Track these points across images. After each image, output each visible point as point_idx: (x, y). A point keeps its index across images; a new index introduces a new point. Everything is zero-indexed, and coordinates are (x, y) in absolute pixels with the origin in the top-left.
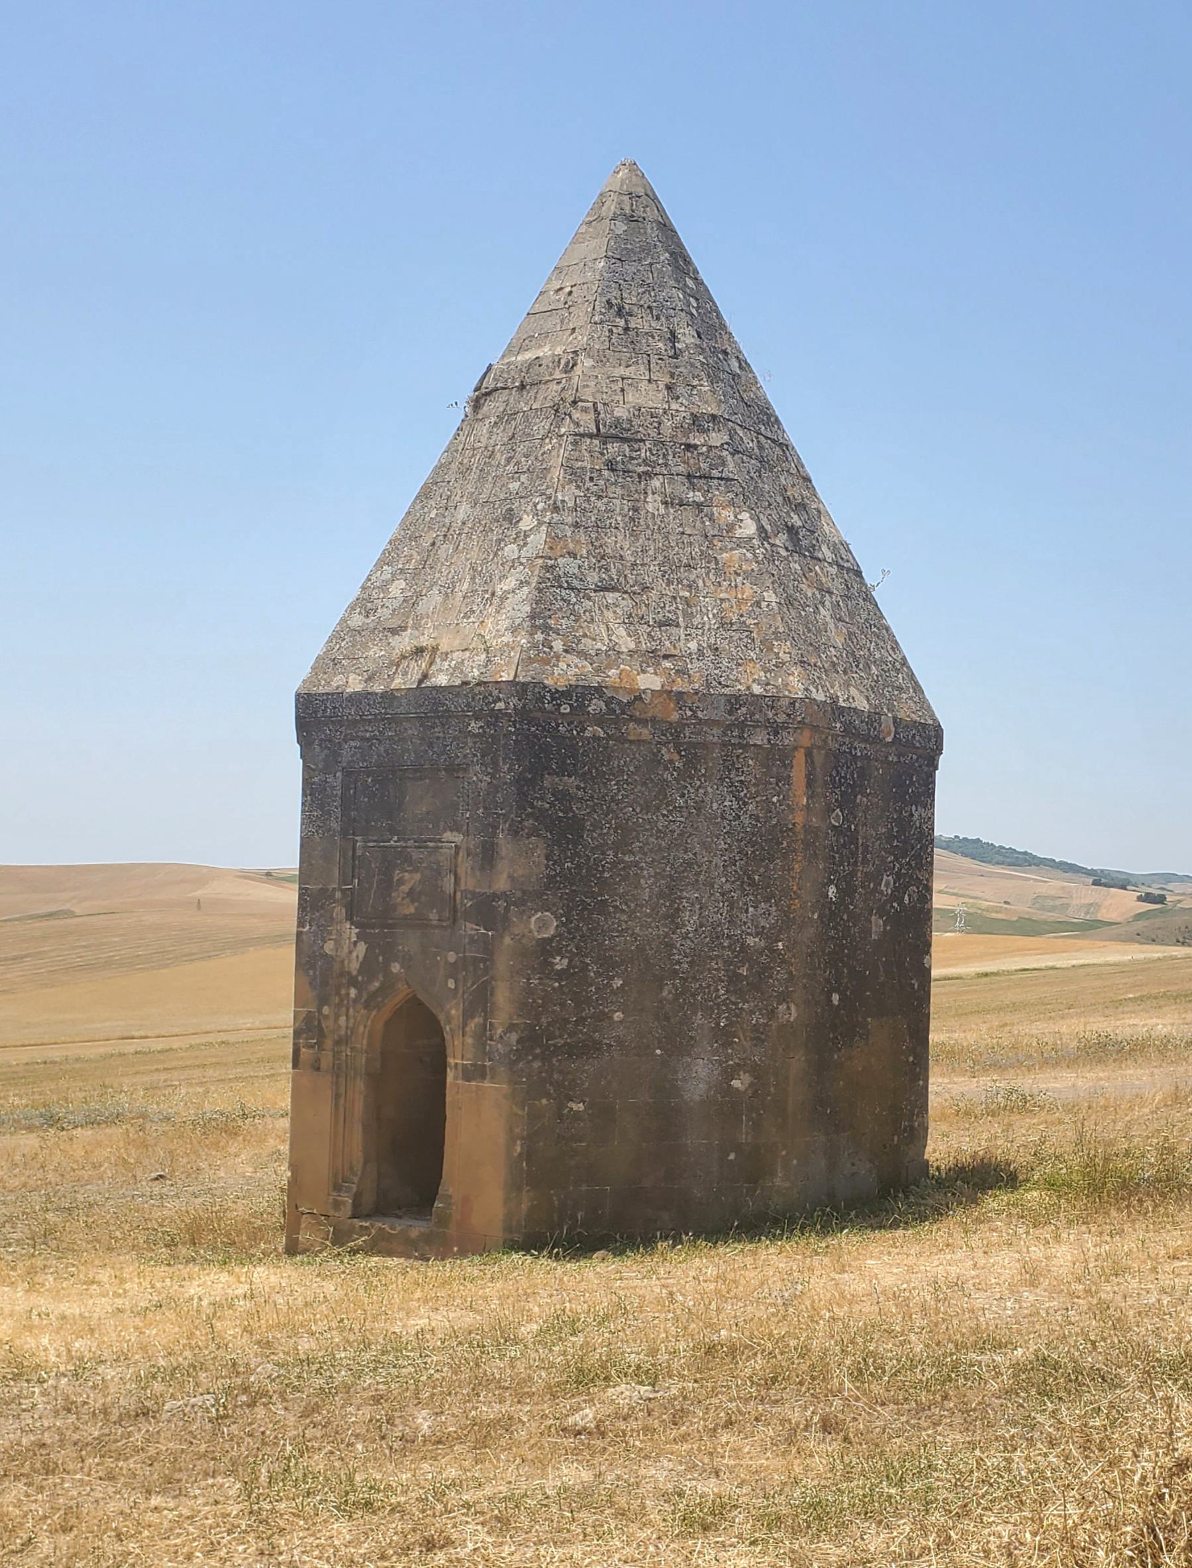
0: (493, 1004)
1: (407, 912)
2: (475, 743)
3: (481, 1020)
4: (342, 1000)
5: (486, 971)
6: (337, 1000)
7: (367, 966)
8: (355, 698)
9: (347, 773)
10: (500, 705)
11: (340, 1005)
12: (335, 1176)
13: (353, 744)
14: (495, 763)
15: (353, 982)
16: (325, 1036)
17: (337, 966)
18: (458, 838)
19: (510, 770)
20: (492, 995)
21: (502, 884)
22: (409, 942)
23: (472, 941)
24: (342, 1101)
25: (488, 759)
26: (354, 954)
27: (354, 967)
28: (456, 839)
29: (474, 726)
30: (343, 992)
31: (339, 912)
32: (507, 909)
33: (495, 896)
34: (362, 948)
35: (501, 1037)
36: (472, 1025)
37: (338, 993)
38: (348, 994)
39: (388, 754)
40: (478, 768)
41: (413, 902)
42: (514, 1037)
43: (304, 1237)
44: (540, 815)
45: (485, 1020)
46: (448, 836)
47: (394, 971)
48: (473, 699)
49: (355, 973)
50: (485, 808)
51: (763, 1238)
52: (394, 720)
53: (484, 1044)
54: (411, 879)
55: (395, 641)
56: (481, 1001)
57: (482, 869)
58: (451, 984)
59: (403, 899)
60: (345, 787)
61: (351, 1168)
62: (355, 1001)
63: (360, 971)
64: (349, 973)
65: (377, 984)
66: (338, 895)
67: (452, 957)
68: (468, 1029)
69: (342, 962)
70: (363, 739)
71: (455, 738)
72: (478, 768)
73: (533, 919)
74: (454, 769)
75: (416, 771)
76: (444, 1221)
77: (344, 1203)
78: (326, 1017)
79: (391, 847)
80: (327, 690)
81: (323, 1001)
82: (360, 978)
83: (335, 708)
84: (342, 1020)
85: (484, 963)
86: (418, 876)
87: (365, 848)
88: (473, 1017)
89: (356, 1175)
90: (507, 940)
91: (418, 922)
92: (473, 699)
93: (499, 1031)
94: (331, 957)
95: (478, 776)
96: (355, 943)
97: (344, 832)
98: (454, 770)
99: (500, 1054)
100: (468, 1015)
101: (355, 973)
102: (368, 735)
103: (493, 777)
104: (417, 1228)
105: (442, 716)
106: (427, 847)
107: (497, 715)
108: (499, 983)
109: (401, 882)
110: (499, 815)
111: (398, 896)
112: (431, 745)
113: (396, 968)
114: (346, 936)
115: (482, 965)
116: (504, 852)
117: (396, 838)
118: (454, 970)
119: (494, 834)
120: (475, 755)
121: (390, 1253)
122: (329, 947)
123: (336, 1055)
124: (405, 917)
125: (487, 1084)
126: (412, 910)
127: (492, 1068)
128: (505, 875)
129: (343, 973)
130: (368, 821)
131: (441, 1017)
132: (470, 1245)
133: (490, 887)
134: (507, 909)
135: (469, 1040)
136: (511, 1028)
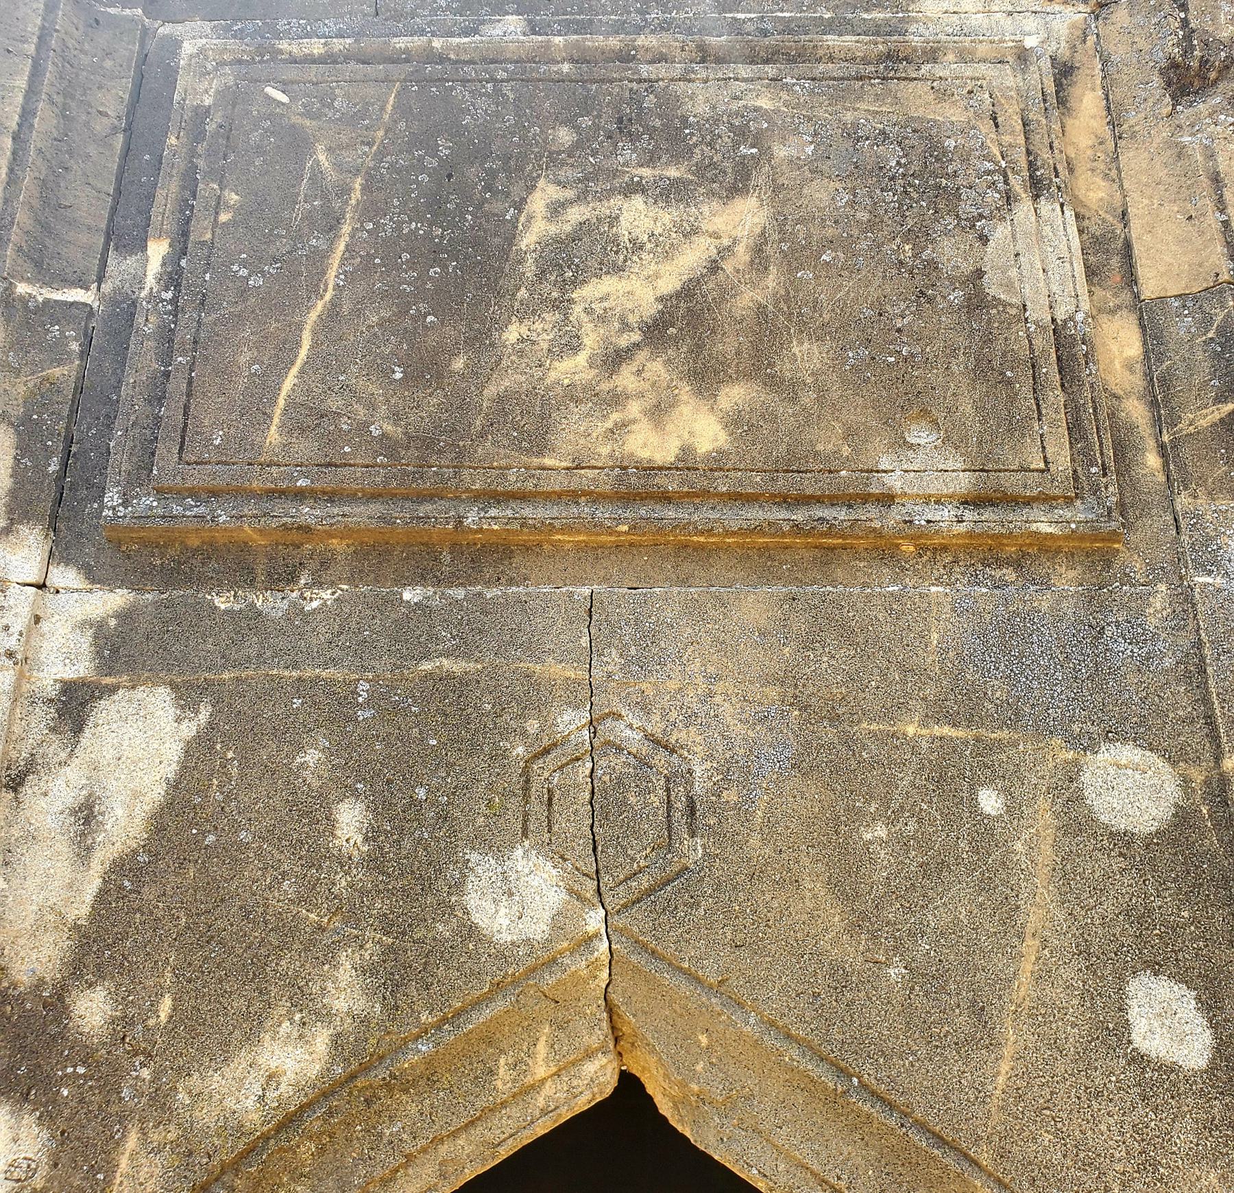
1: (650, 445)
22: (697, 678)
41: (705, 378)
54: (668, 244)
59: (614, 359)
63: (98, 947)
65: (293, 1056)
82: (92, 1010)
86: (742, 219)
91: (798, 524)
96: (74, 706)
109: (573, 259)
113: (520, 897)
124: (638, 487)
126: (702, 429)
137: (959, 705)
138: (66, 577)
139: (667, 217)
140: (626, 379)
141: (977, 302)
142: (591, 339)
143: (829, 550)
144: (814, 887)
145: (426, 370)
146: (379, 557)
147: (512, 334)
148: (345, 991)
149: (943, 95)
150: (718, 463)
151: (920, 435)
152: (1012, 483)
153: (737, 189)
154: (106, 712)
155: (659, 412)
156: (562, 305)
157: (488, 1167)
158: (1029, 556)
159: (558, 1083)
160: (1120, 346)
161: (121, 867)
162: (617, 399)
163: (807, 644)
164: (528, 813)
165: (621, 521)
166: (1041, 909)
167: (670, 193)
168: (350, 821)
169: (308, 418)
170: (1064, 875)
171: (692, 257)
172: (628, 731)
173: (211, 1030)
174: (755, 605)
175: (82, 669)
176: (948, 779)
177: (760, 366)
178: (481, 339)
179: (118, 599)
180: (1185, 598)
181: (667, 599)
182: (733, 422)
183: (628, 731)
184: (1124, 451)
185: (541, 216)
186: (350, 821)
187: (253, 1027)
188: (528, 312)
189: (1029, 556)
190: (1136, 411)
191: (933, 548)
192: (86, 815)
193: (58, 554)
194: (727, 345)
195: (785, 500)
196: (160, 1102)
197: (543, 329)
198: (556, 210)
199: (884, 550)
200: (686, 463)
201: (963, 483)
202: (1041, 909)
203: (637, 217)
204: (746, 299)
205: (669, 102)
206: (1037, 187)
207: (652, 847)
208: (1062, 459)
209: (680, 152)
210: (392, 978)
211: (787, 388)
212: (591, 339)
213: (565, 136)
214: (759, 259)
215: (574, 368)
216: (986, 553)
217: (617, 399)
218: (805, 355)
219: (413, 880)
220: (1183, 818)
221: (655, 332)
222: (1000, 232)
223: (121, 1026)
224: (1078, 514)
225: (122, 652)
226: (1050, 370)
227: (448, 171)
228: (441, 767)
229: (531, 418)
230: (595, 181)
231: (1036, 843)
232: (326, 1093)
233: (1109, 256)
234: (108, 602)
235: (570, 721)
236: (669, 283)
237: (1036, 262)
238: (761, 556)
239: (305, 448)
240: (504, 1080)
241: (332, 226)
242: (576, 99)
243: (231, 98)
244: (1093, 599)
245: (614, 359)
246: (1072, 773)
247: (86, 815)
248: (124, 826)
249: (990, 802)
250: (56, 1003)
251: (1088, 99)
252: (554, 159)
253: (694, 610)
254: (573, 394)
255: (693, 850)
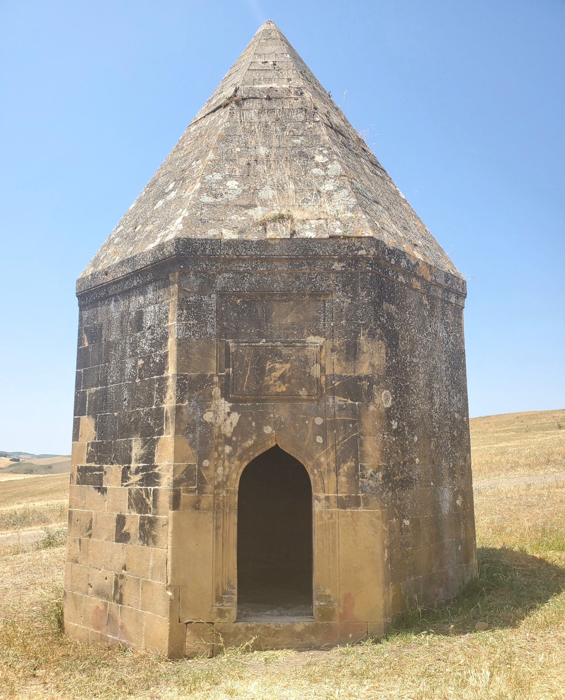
0: (362, 452)
1: (279, 390)
2: (337, 277)
3: (353, 464)
4: (219, 455)
5: (355, 429)
6: (216, 455)
7: (239, 430)
8: (230, 244)
9: (222, 294)
10: (362, 252)
11: (219, 458)
12: (217, 589)
13: (226, 275)
14: (355, 292)
15: (228, 441)
16: (206, 483)
17: (216, 431)
18: (320, 340)
19: (368, 295)
20: (361, 445)
21: (364, 370)
22: (281, 412)
23: (341, 408)
24: (220, 531)
25: (348, 288)
26: (228, 422)
27: (228, 430)
28: (319, 341)
29: (337, 266)
30: (220, 449)
31: (217, 391)
32: (370, 387)
33: (360, 378)
34: (235, 417)
35: (371, 475)
36: (345, 468)
37: (216, 450)
38: (223, 450)
39: (259, 283)
40: (340, 293)
41: (284, 383)
42: (380, 475)
43: (190, 643)
44: (382, 326)
45: (357, 463)
46: (311, 339)
47: (266, 432)
48: (339, 247)
49: (229, 435)
50: (347, 320)
51: (347, 645)
52: (268, 260)
53: (357, 482)
54: (281, 368)
55: (251, 212)
56: (353, 449)
57: (347, 360)
58: (319, 439)
59: (275, 381)
60: (219, 305)
61: (229, 585)
62: (230, 456)
63: (234, 434)
64: (225, 435)
65: (250, 442)
66: (216, 379)
67: (319, 421)
68: (341, 471)
69: (220, 427)
70: (236, 272)
71: (319, 274)
72: (340, 293)
73: (383, 394)
74: (316, 294)
75: (283, 295)
76: (327, 614)
77: (229, 611)
78: (207, 468)
79: (262, 346)
80: (203, 237)
81: (202, 456)
82: (234, 439)
83: (213, 249)
84: (220, 470)
85: (353, 424)
86: (288, 366)
87: (238, 347)
88: (345, 462)
89: (234, 588)
90: (372, 408)
91: (291, 397)
92: (339, 247)
93: (370, 471)
94: (211, 423)
95: (340, 299)
96: (229, 414)
97: (219, 336)
98: (317, 295)
99: (371, 487)
100: (340, 461)
101: (229, 435)
102: (241, 269)
103: (353, 299)
104: (300, 624)
105: (311, 258)
106: (294, 346)
107: (357, 259)
108: (367, 437)
109: (273, 370)
110: (359, 325)
111: (270, 380)
112: (297, 278)
113: (268, 430)
114: (221, 409)
115: (351, 425)
116: (365, 349)
117: (264, 340)
118: (322, 430)
119: (356, 337)
120: (337, 285)
121: (276, 647)
122: (208, 417)
123: (216, 496)
124: (278, 394)
125: (361, 510)
126: (284, 388)
127: (365, 498)
128: (367, 364)
129: (220, 436)
130: (237, 329)
131: (309, 466)
132: (331, 633)
133: (354, 372)
134: (370, 387)
135: (343, 479)
136: (378, 469)
137: (305, 414)
138: (226, 402)
139: (281, 365)
140: (276, 383)
141: (310, 375)
142: (273, 379)
143: (295, 400)
144: (292, 429)
145: (258, 382)
146: (254, 401)
147: (266, 379)
148: (254, 437)
149: (308, 351)
150: (285, 392)
151: (304, 389)
152: (311, 394)
153: (287, 363)
154: (232, 414)
155: (280, 387)
156: (270, 375)
157: (260, 452)
158: (312, 401)
159: (271, 444)
160: (323, 379)
161: (235, 428)
162: (276, 385)
163: (293, 409)
164: (269, 423)
165: (276, 397)
166: (310, 431)
167: (281, 363)
168: (254, 424)
169: (247, 387)
170: (312, 428)
171: (283, 370)
172: (277, 416)
173: (244, 440)
174: (288, 405)
175: (229, 411)
176: (304, 420)
177: (289, 382)
178: (263, 379)
179: (231, 404)
180: (325, 404)
181: (280, 405)
182: (286, 388)
183: (277, 416)
184: (322, 390)
185: (268, 365)
186: (254, 424)
187: (247, 440)
188: (267, 376)
189: (312, 401)
190: (324, 386)
191: (304, 400)
192: (231, 423)
193: (226, 400)
194: (286, 380)
195: (291, 396)
196: (240, 446)
197: (268, 378)
198: (270, 365)
199: (300, 400)
200: (282, 392)
201: (307, 394)
202: (310, 431)
203: (278, 366)
204: (288, 375)
205: (281, 352)
206: (317, 362)
207: (277, 425)
208: (316, 392)
209: (282, 358)
210: (258, 436)
211: (292, 384)
212: (273, 379)
213: (270, 356)
214: (289, 371)
215: (271, 382)
216: (308, 400)
217: (276, 385)
218: (293, 381)
219: (259, 429)
220: (323, 423)
221: (279, 378)
222: (313, 368)
223: (237, 440)
224: (316, 397)
225: (232, 409)
226: (316, 383)
227: (259, 360)
228: (262, 419)
229: (268, 387)
230: (274, 362)
231: (310, 426)
232: (253, 445)
233: (323, 370)
234: (230, 404)
235: (272, 415)
236: (281, 373)
237: (316, 371)
238: (289, 401)
239: (247, 390)
240: (267, 444)
241: (248, 367)
242: (271, 351)
243: (236, 351)
244: (318, 405)
245: (275, 381)
246: (314, 420)
247: (231, 423)
248: (235, 424)
249: (307, 422)
250: (231, 438)
251: (324, 351)
252: (269, 359)
253: (283, 405)
254: (272, 385)
255: (282, 426)
